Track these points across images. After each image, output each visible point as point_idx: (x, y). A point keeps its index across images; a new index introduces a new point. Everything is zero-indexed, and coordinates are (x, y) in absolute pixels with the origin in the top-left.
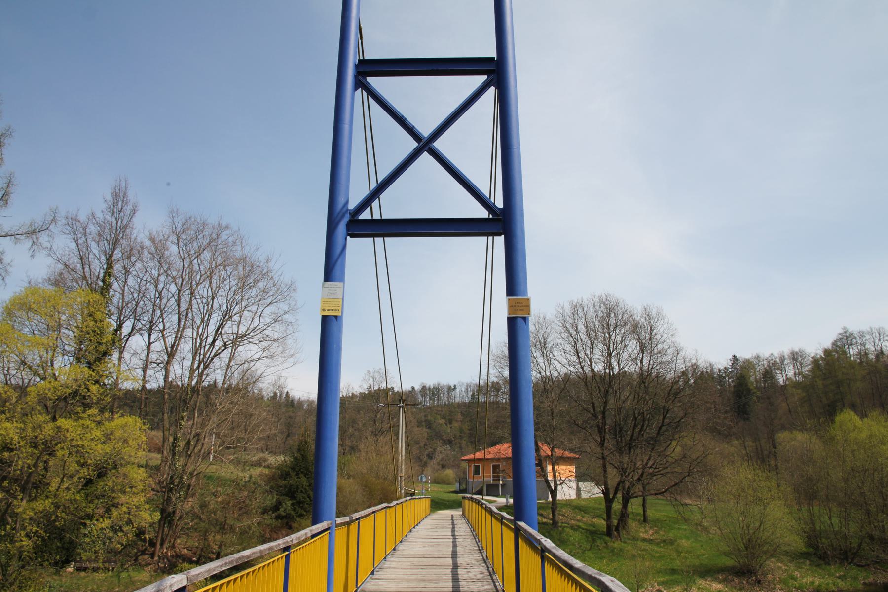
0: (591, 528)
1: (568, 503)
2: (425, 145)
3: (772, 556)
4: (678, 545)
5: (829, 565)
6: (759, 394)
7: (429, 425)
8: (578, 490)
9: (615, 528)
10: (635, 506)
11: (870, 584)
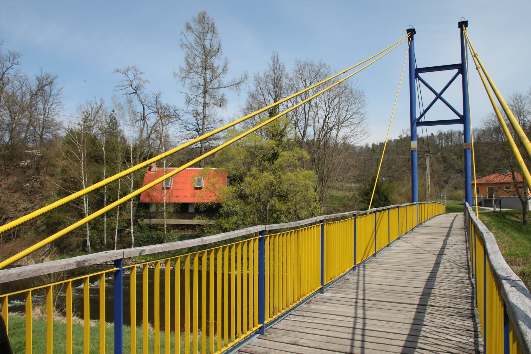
2: (439, 96)
7: (445, 160)
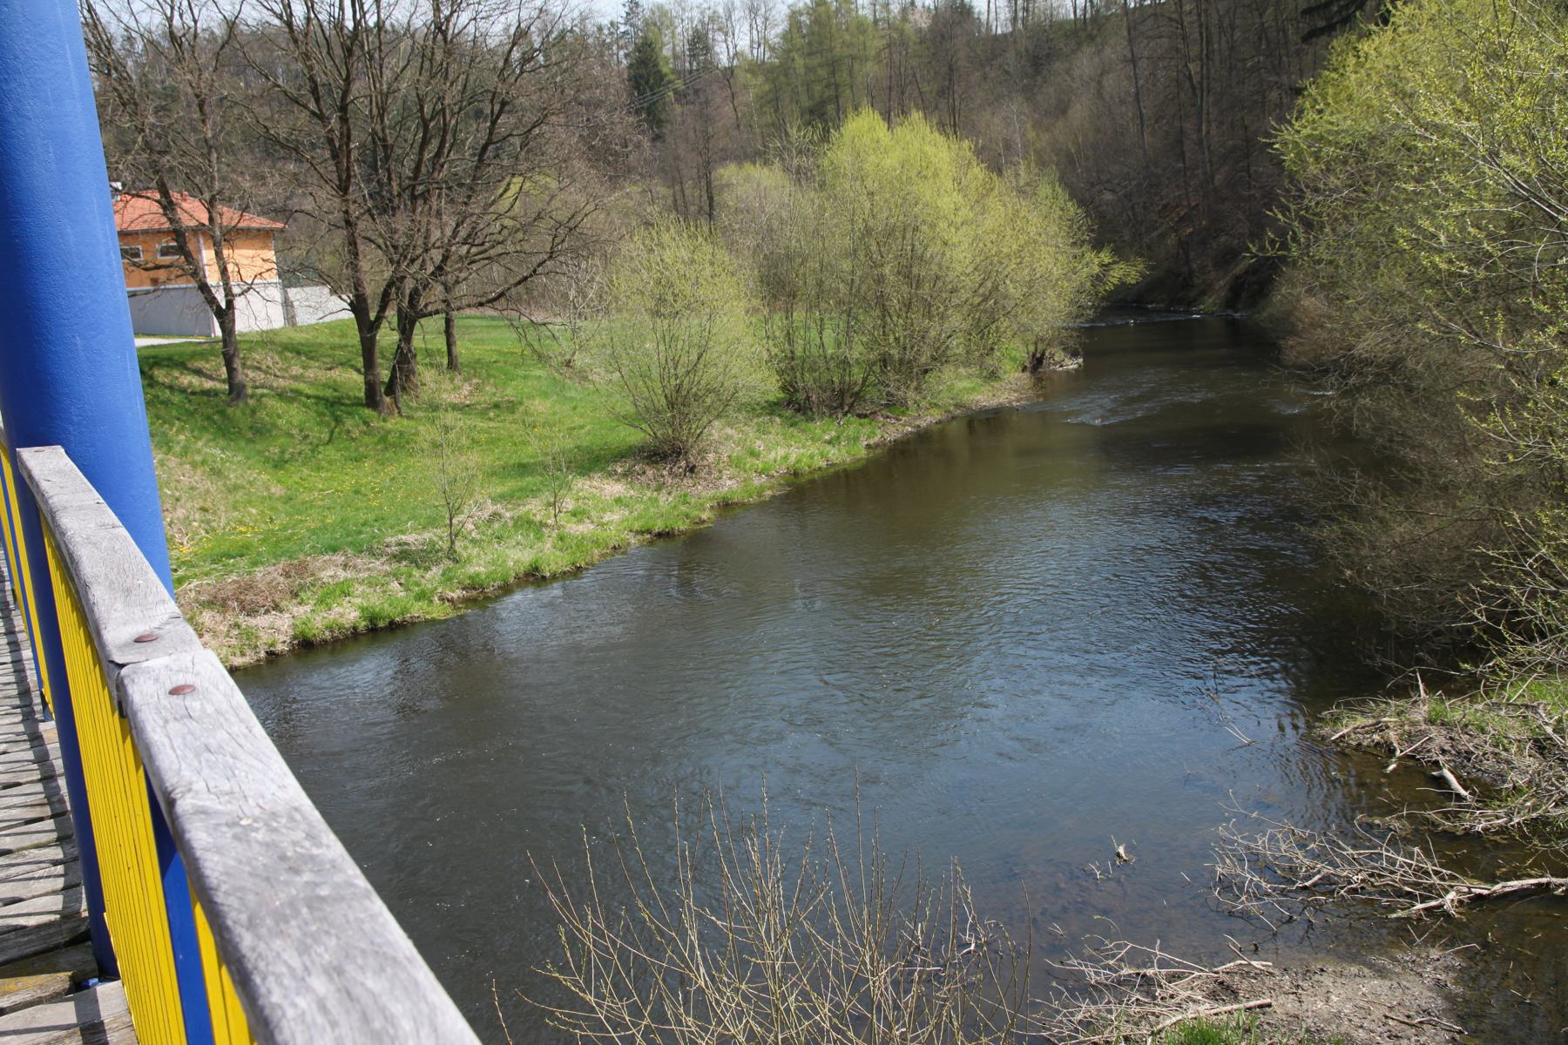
0: (328, 393)
1: (267, 340)
3: (718, 417)
4: (526, 412)
5: (812, 420)
6: (679, 84)
8: (287, 304)
9: (388, 385)
10: (428, 334)
11: (877, 445)
